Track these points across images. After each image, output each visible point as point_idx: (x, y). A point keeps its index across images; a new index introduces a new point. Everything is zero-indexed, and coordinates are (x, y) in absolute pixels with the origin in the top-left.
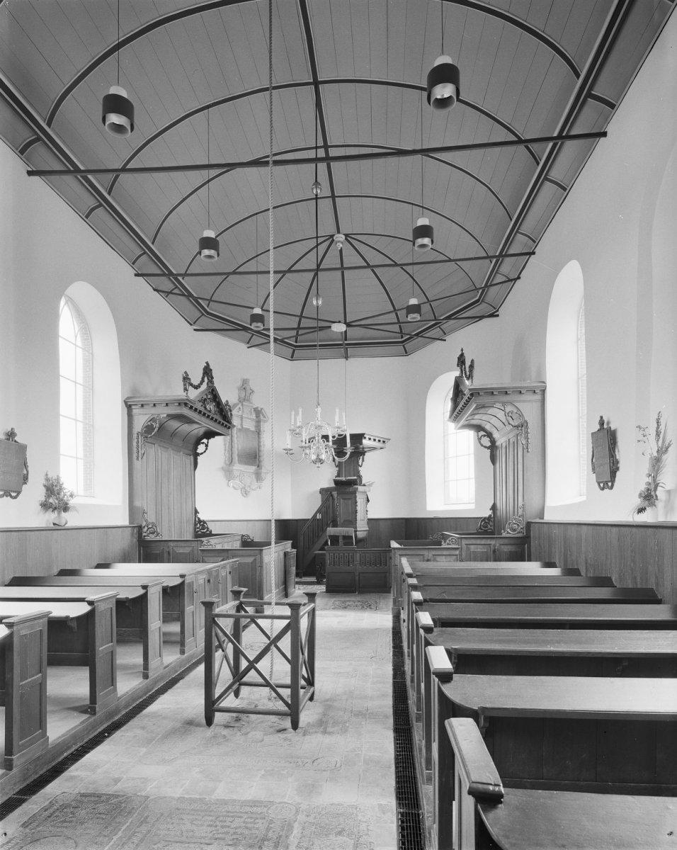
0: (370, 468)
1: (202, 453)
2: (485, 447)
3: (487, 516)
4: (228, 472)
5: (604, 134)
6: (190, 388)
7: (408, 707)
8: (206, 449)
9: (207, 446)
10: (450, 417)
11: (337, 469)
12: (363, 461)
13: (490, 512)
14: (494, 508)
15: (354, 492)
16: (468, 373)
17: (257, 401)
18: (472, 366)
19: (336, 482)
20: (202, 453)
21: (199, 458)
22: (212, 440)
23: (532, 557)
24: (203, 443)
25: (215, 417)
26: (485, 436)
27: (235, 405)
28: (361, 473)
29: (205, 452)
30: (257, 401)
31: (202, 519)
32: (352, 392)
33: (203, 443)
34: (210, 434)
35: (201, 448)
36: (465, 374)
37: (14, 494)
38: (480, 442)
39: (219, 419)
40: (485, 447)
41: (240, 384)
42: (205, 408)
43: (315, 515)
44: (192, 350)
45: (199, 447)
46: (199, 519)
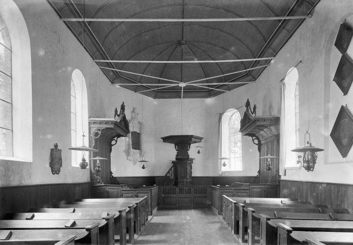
0: (193, 151)
1: (114, 145)
2: (256, 144)
3: (256, 176)
4: (128, 153)
5: (268, 5)
6: (116, 116)
7: (117, 220)
8: (116, 143)
9: (116, 141)
10: (241, 129)
11: (177, 152)
12: (190, 148)
13: (258, 174)
14: (259, 172)
15: (186, 164)
16: (252, 111)
17: (140, 118)
18: (255, 108)
19: (177, 159)
20: (114, 145)
21: (113, 147)
22: (119, 139)
23: (280, 195)
24: (114, 140)
25: (123, 128)
26: (255, 139)
27: (130, 121)
28: (189, 154)
29: (115, 144)
30: (140, 118)
31: (114, 176)
32: (184, 115)
33: (114, 140)
34: (119, 136)
35: (113, 142)
36: (251, 111)
37: (312, 169)
38: (253, 142)
39: (124, 129)
40: (256, 144)
41: (132, 110)
42: (120, 124)
43: (167, 174)
44: (121, 95)
45: (112, 141)
46: (113, 176)
